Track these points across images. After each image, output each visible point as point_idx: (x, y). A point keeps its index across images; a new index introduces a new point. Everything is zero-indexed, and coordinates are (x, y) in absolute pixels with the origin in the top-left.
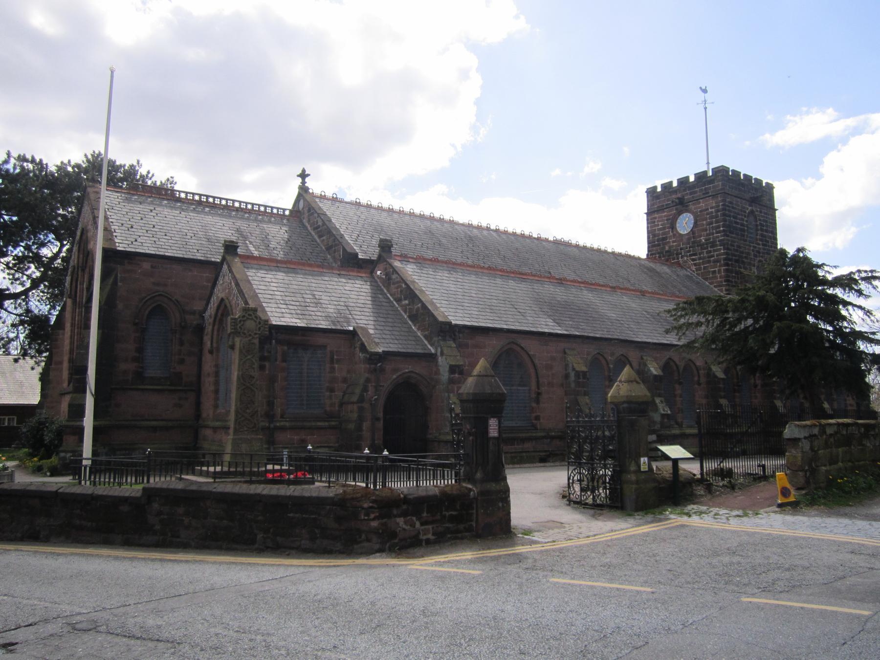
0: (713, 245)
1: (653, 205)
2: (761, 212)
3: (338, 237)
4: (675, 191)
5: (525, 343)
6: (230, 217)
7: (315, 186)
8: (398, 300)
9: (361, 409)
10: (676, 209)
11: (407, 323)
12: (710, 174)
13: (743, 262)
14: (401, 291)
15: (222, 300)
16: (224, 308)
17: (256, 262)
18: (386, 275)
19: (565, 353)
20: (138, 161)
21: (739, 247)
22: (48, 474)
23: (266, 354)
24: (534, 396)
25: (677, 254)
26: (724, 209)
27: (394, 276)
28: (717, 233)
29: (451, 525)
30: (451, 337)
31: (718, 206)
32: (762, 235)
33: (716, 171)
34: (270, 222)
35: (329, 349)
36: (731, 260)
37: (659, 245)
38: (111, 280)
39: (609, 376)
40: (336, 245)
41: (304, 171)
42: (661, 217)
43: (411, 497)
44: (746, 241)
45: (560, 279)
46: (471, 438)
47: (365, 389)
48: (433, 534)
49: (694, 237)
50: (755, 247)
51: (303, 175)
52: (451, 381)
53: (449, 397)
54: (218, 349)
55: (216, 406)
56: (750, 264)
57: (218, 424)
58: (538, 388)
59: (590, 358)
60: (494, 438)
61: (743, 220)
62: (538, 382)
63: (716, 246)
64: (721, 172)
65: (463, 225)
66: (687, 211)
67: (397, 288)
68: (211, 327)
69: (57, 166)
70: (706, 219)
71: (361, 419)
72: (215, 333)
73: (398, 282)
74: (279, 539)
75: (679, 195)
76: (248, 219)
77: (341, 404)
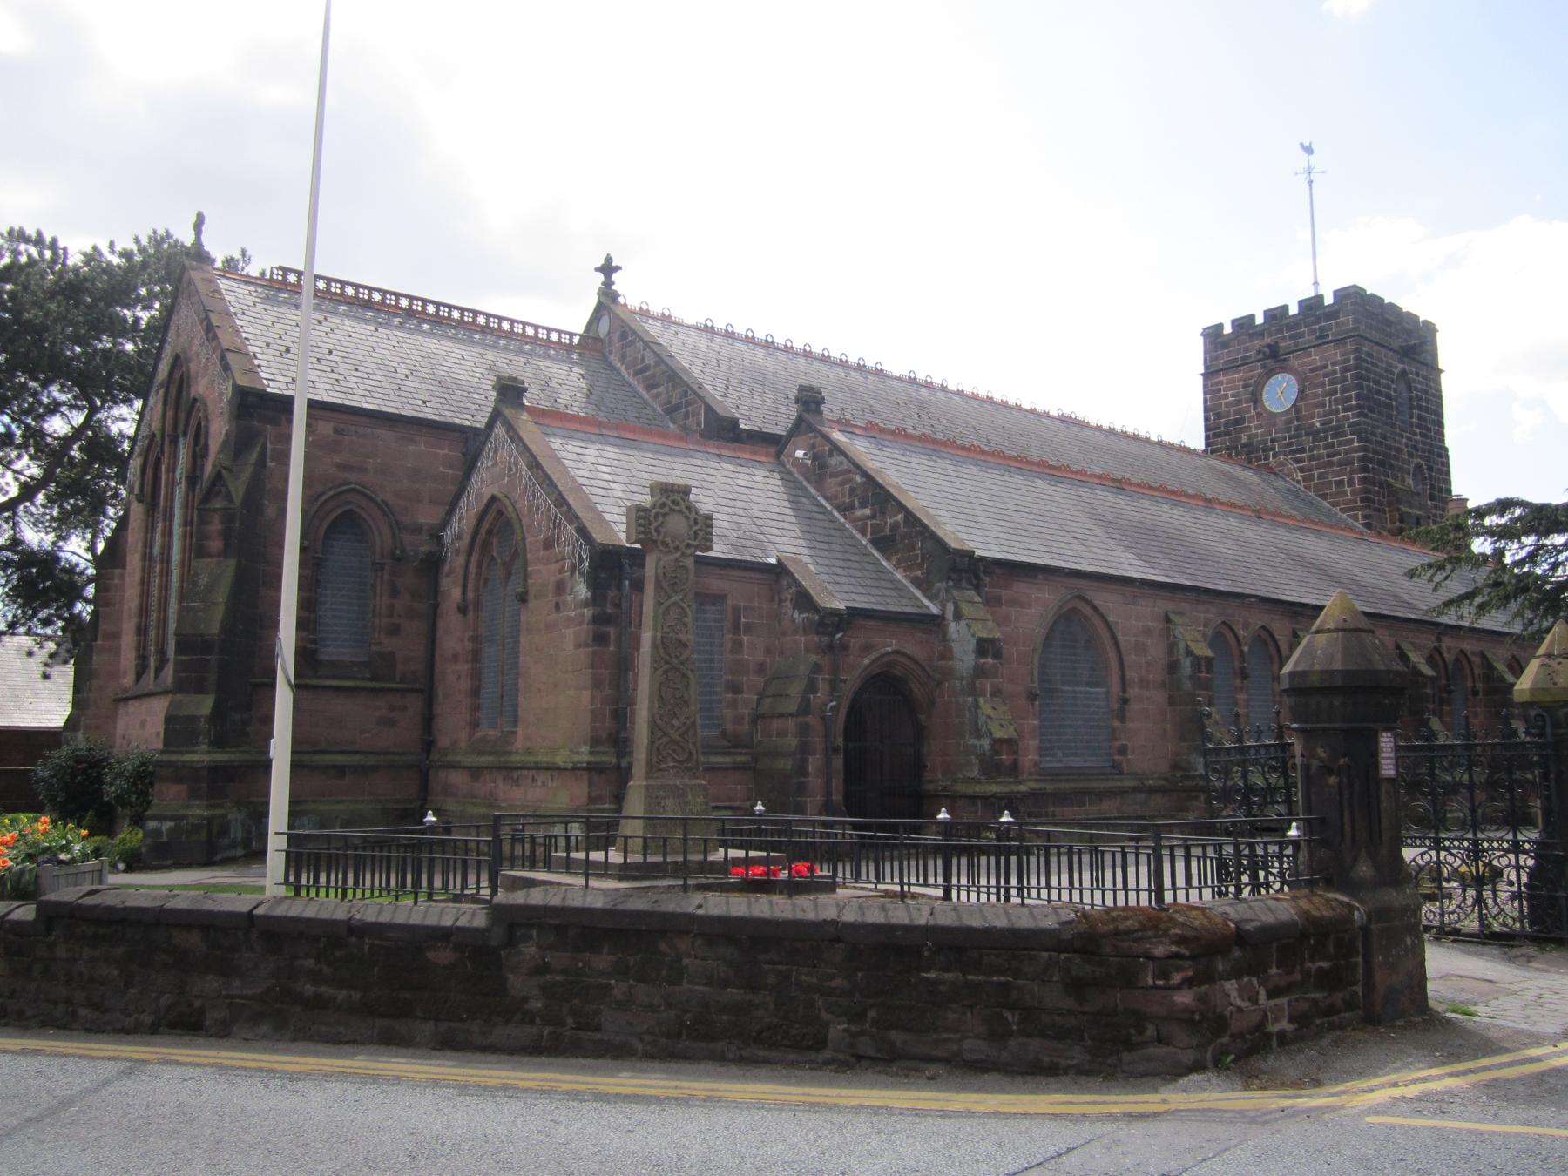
0: (1338, 432)
2: (1417, 374)
3: (695, 387)
5: (1107, 601)
6: (471, 342)
7: (632, 291)
8: (846, 509)
9: (804, 730)
10: (1263, 366)
13: (1391, 467)
14: (852, 490)
15: (493, 499)
16: (497, 522)
17: (559, 424)
18: (815, 458)
20: (244, 252)
21: (1385, 438)
22: (121, 866)
24: (1116, 706)
25: (1265, 450)
26: (1357, 367)
27: (835, 460)
28: (1345, 410)
29: (1318, 995)
30: (969, 582)
31: (1348, 360)
32: (1420, 418)
33: (1341, 295)
35: (729, 602)
36: (1371, 461)
37: (1228, 433)
38: (253, 457)
39: (1243, 669)
40: (688, 404)
41: (609, 260)
42: (1233, 381)
43: (1249, 927)
44: (1393, 426)
45: (1119, 481)
47: (812, 687)
48: (1291, 1020)
49: (1298, 419)
51: (608, 269)
53: (977, 706)
54: (478, 605)
55: (474, 724)
56: (1401, 469)
57: (483, 760)
58: (1124, 691)
59: (1210, 632)
60: (1390, 780)
62: (1123, 678)
63: (1344, 434)
64: (1353, 298)
65: (899, 379)
66: (1284, 370)
67: (842, 484)
68: (461, 560)
69: (85, 254)
70: (1323, 385)
71: (804, 749)
74: (897, 1037)
75: (1268, 340)
76: (505, 349)
77: (756, 718)
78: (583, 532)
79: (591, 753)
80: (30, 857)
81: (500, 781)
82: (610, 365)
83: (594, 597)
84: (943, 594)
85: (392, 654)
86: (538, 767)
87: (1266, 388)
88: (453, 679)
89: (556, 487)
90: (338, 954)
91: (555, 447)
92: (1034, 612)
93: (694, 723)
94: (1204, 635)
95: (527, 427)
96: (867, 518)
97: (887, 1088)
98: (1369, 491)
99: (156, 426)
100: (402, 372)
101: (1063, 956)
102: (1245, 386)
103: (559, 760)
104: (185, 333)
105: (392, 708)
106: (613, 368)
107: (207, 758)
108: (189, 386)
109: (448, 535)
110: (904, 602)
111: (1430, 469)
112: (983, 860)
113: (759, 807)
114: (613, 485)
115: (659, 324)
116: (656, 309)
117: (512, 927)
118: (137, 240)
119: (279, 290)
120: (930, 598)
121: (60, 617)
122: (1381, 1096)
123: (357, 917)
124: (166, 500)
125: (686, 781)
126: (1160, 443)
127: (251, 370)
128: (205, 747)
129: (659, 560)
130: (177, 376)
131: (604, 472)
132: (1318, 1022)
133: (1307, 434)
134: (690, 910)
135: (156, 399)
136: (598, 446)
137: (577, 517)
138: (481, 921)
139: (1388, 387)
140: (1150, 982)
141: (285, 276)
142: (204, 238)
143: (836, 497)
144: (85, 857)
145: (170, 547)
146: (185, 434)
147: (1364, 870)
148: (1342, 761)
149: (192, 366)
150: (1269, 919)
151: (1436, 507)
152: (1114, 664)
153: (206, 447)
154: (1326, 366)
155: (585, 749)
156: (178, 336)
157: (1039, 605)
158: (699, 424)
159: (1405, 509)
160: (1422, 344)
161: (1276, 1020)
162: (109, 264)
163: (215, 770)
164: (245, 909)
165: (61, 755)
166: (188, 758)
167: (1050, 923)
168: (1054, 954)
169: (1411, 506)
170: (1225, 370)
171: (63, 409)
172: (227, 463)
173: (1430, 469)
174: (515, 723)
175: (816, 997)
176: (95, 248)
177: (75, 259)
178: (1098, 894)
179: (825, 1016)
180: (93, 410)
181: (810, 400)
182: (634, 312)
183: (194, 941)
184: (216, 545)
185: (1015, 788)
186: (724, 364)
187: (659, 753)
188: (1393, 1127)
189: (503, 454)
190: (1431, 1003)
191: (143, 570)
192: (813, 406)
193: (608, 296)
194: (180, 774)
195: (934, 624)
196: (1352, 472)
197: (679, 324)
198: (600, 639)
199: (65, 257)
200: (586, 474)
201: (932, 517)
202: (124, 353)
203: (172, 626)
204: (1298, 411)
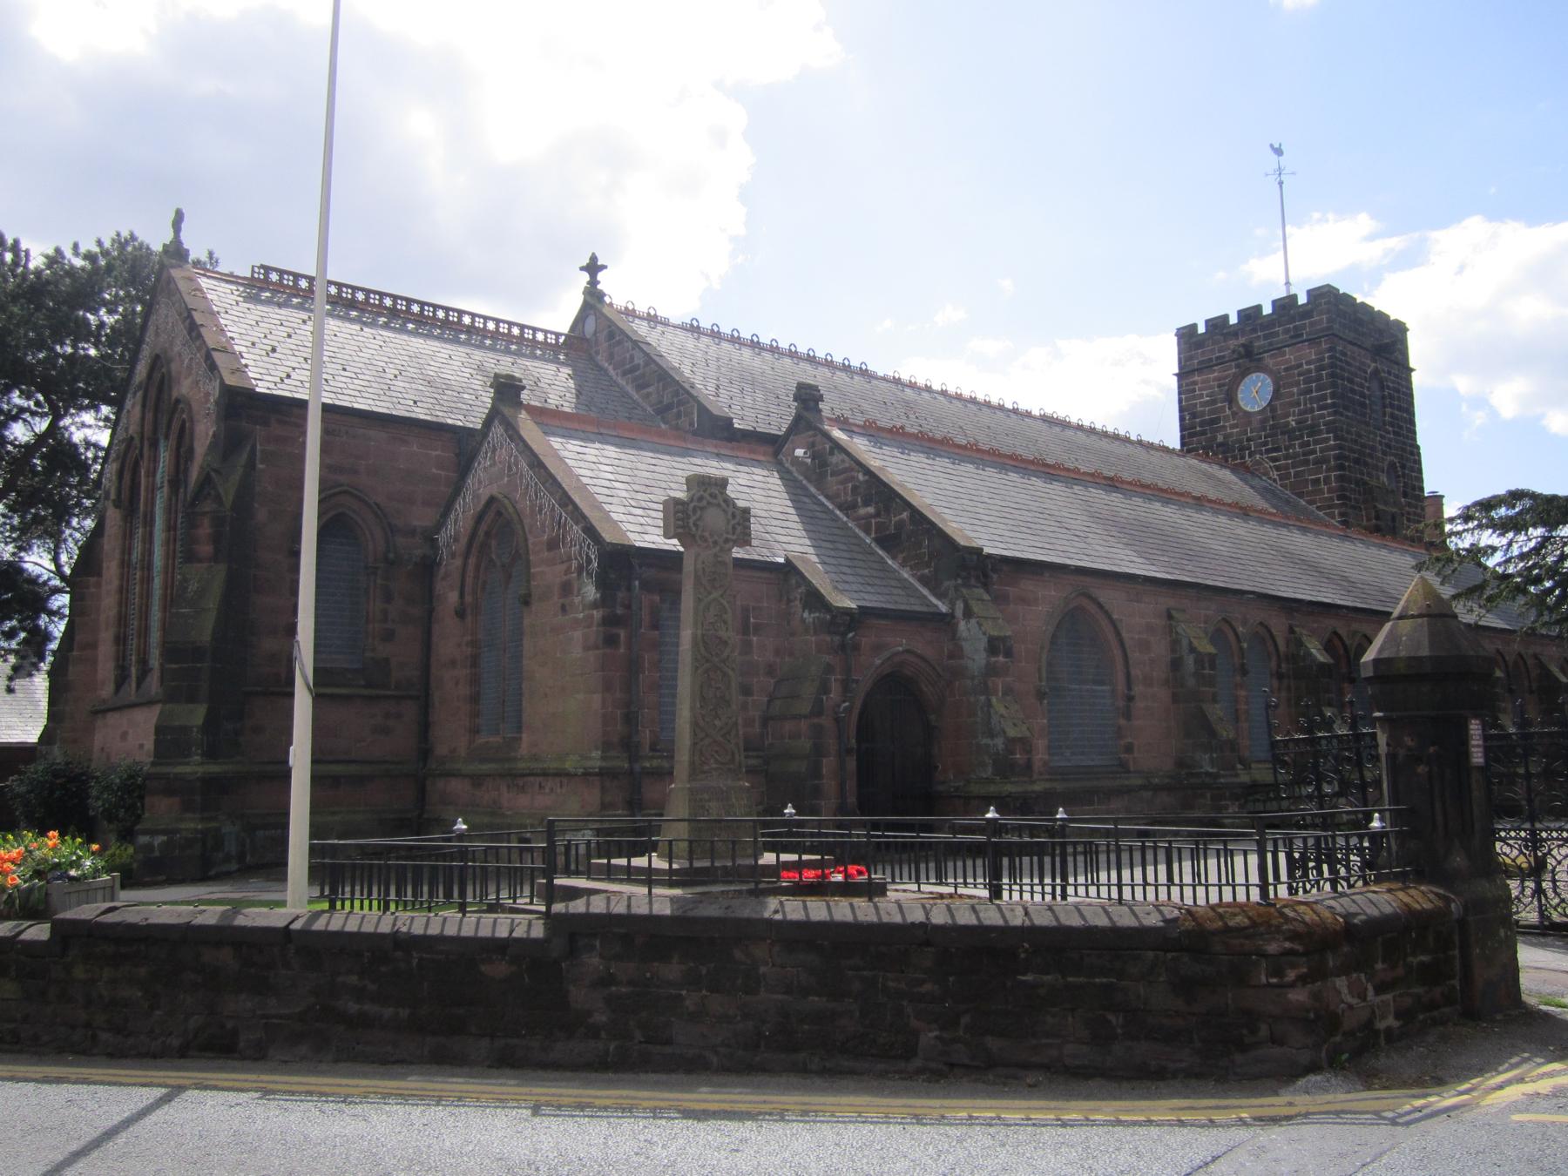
0: (1313, 430)
1: (1191, 358)
3: (687, 386)
4: (1234, 332)
5: (1110, 597)
7: (618, 290)
8: (848, 508)
10: (1238, 366)
11: (874, 553)
13: (1366, 464)
14: (855, 488)
15: (492, 500)
16: (497, 523)
20: (211, 254)
21: (1360, 436)
23: (619, 611)
24: (1121, 703)
25: (1242, 449)
26: (1332, 366)
28: (1321, 408)
31: (1323, 359)
32: (1392, 416)
34: (534, 357)
37: (1203, 433)
39: (1243, 665)
40: (680, 403)
41: (594, 258)
42: (1207, 381)
44: (1367, 424)
45: (1111, 479)
48: (1397, 1017)
51: (593, 268)
53: (990, 705)
57: (486, 767)
58: (1129, 688)
62: (1128, 676)
63: (1320, 432)
64: (1328, 300)
65: (884, 379)
66: (1259, 369)
68: (458, 562)
69: (47, 257)
70: (1297, 384)
73: (845, 470)
74: (993, 1043)
75: (1242, 340)
76: (492, 349)
77: (766, 720)
78: (591, 531)
79: (603, 758)
80: (38, 874)
82: (597, 365)
83: (603, 598)
84: (951, 593)
85: (387, 660)
86: (545, 774)
87: (1241, 387)
88: (451, 685)
89: (560, 486)
90: (383, 969)
91: (556, 446)
92: (1038, 613)
93: (736, 724)
94: (1206, 633)
95: (527, 427)
96: (872, 516)
97: (990, 1097)
99: (133, 429)
100: (391, 372)
101: (1169, 955)
103: (569, 765)
104: (164, 333)
106: (600, 369)
107: (200, 769)
108: (170, 388)
109: (442, 537)
110: (912, 600)
111: (1403, 467)
112: (1026, 860)
113: (789, 810)
115: (645, 323)
116: (642, 307)
118: (99, 243)
119: (262, 289)
120: (939, 596)
121: (24, 629)
122: (1514, 1092)
123: (404, 929)
124: (146, 504)
125: (729, 782)
126: (1140, 443)
127: (238, 370)
128: (197, 758)
129: (698, 555)
130: (157, 376)
131: (606, 472)
132: (1421, 1017)
133: (1283, 433)
134: (766, 915)
135: (133, 403)
136: (597, 445)
137: (584, 517)
138: (538, 931)
140: (1263, 979)
141: (266, 275)
142: (183, 236)
144: (96, 872)
145: (150, 553)
146: (167, 437)
147: (1458, 860)
148: (1432, 750)
149: (174, 367)
150: (1373, 912)
151: (1409, 505)
152: (1120, 665)
153: (191, 450)
154: (1300, 365)
155: (596, 754)
156: (157, 334)
157: (1046, 601)
158: (691, 424)
159: (1381, 507)
160: (1394, 343)
161: (1383, 1017)
162: (72, 267)
163: (209, 782)
164: (281, 924)
165: (37, 769)
166: (179, 769)
167: (1153, 920)
168: (1161, 953)
169: (1386, 504)
170: (1199, 370)
171: (26, 416)
173: (1403, 467)
174: (519, 729)
175: (905, 1003)
176: (58, 251)
177: (36, 262)
178: (1201, 891)
179: (914, 1023)
180: (57, 417)
181: (807, 397)
182: (620, 312)
183: (226, 956)
184: (206, 549)
185: (1030, 788)
186: (713, 364)
187: (701, 754)
188: (1544, 1125)
189: (502, 454)
190: (1524, 997)
191: (122, 579)
192: (812, 404)
193: (593, 297)
194: (172, 787)
195: (944, 622)
196: (1328, 470)
197: (666, 323)
198: (611, 641)
199: (27, 260)
200: (589, 473)
201: (939, 515)
202: (88, 357)
203: (155, 636)
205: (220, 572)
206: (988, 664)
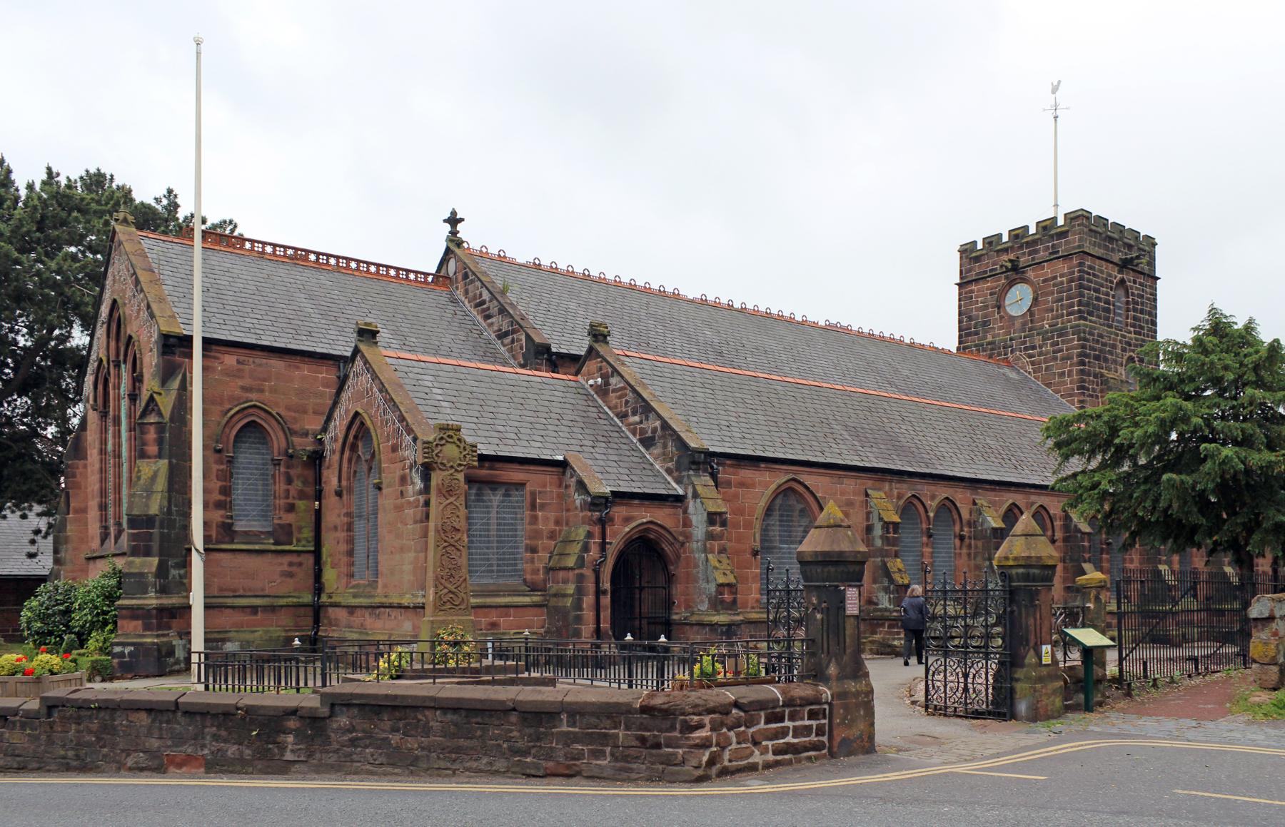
2: (1135, 282)
5: (811, 479)
8: (623, 416)
9: (581, 578)
10: (1007, 278)
12: (1061, 222)
13: (1106, 360)
14: (627, 402)
19: (867, 495)
26: (1081, 278)
32: (1135, 318)
36: (1087, 356)
38: (176, 384)
40: (514, 332)
41: (454, 213)
46: (819, 616)
47: (586, 548)
49: (1032, 321)
50: (1124, 336)
51: (454, 220)
52: (710, 536)
53: (707, 560)
54: (350, 490)
56: (1115, 362)
59: (901, 502)
61: (1107, 294)
63: (1066, 334)
64: (1080, 218)
67: (620, 397)
68: (336, 457)
71: (580, 592)
72: (345, 465)
75: (1012, 256)
81: (367, 615)
85: (290, 525)
86: (391, 606)
98: (1084, 381)
102: (991, 294)
105: (291, 564)
113: (629, 637)
114: (444, 404)
117: (333, 705)
128: (153, 595)
139: (1107, 294)
143: (616, 407)
145: (120, 446)
146: (125, 362)
153: (141, 375)
163: (161, 610)
172: (156, 389)
174: (377, 575)
184: (152, 449)
192: (601, 338)
193: (455, 241)
204: (1032, 315)
205: (163, 464)
206: (707, 532)
